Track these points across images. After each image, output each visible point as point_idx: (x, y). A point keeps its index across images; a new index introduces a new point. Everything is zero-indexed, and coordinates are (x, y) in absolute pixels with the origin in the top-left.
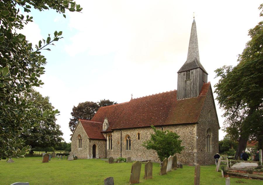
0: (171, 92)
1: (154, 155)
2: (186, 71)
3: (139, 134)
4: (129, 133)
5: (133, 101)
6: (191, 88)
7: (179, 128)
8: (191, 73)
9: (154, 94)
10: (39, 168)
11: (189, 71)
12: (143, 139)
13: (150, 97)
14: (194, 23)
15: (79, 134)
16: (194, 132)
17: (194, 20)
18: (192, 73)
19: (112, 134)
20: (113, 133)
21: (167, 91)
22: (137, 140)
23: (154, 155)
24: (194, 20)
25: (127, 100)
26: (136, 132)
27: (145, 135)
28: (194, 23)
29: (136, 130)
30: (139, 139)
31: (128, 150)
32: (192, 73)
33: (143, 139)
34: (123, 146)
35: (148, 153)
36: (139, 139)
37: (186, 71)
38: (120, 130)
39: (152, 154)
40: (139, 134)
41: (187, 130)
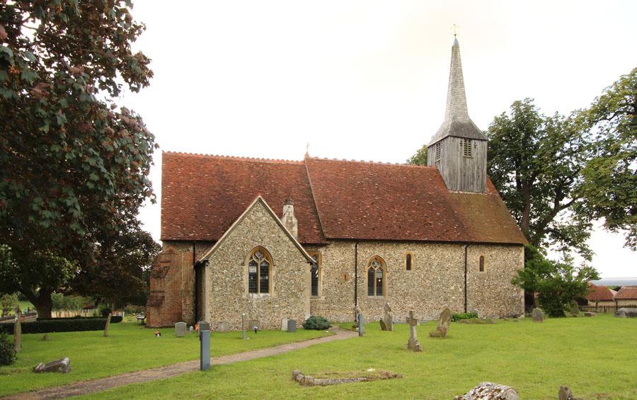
0: (388, 166)
1: (446, 305)
2: (466, 139)
3: (409, 258)
4: (379, 251)
5: (309, 160)
6: (473, 174)
7: (496, 251)
8: (473, 147)
9: (384, 162)
10: (612, 358)
11: (470, 139)
12: (419, 268)
13: (371, 166)
14: (455, 49)
15: (257, 244)
16: (521, 261)
17: (456, 40)
18: (475, 146)
19: (322, 251)
20: (324, 249)
21: (335, 157)
22: (405, 271)
23: (446, 305)
24: (456, 40)
25: (298, 157)
26: (400, 252)
27: (424, 259)
28: (455, 49)
29: (402, 246)
30: (409, 267)
31: (375, 297)
32: (475, 146)
33: (419, 268)
34: (360, 286)
35: (431, 301)
36: (409, 267)
37: (466, 139)
38: (357, 241)
39: (442, 302)
40: (409, 258)
41: (510, 256)
